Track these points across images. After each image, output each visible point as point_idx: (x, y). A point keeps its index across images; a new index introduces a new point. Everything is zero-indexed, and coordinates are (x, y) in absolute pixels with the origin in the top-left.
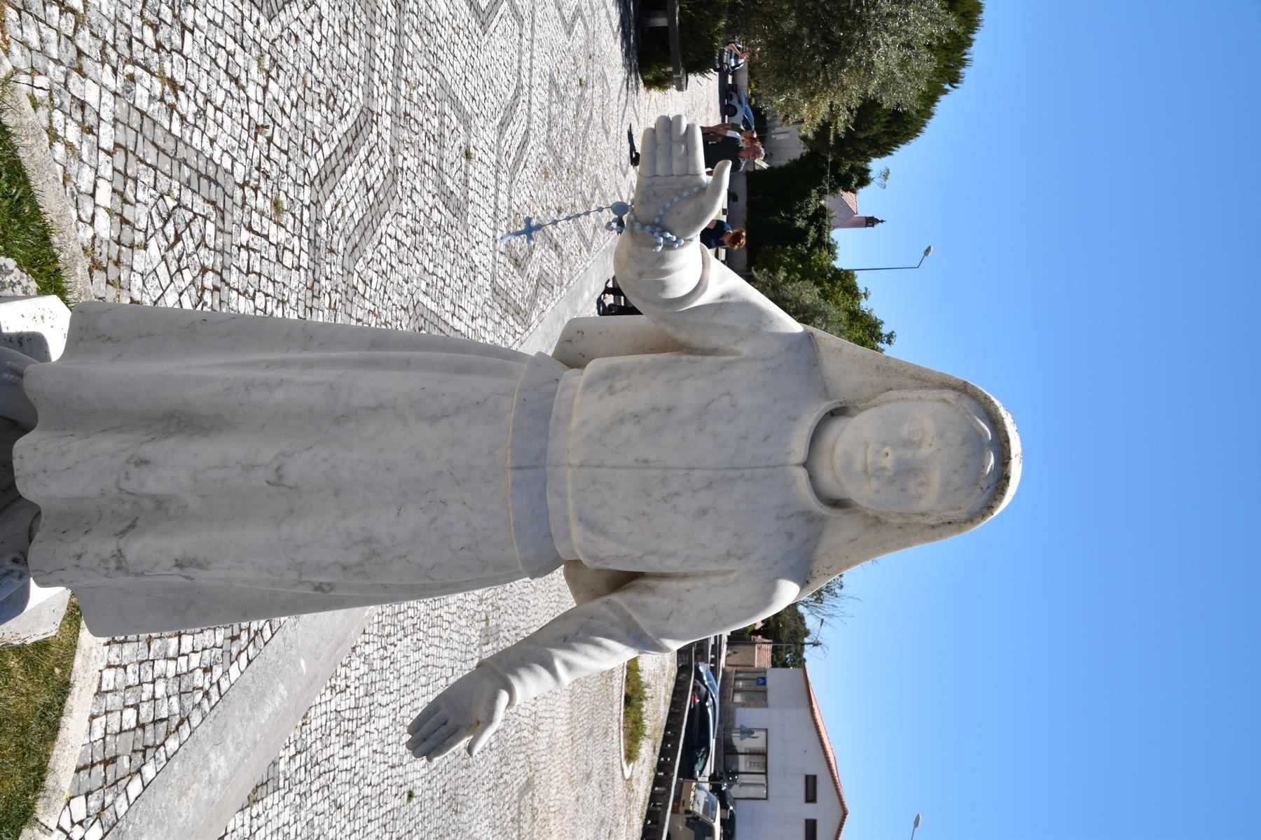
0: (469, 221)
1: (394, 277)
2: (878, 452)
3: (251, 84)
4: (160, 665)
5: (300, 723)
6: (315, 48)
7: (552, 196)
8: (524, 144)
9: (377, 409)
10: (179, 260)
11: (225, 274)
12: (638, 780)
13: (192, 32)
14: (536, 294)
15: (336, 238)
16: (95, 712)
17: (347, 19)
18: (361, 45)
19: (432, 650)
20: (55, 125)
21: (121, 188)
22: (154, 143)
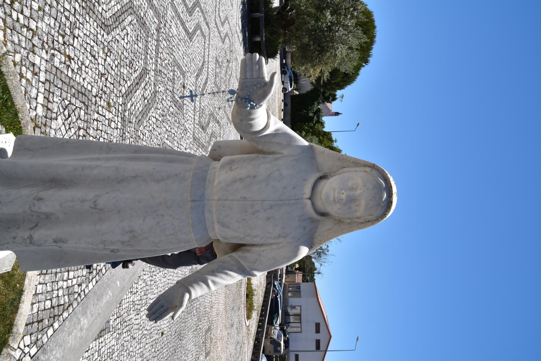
0: (184, 112)
1: (155, 133)
2: (339, 193)
3: (100, 58)
4: (61, 283)
5: (118, 306)
6: (125, 45)
7: (217, 103)
8: (206, 83)
9: (135, 177)
10: (70, 124)
11: (88, 130)
12: (252, 326)
13: (77, 38)
14: (210, 140)
15: (132, 117)
16: (34, 301)
17: (138, 35)
18: (143, 44)
19: (170, 277)
20: (23, 72)
21: (47, 97)
22: (61, 80)
